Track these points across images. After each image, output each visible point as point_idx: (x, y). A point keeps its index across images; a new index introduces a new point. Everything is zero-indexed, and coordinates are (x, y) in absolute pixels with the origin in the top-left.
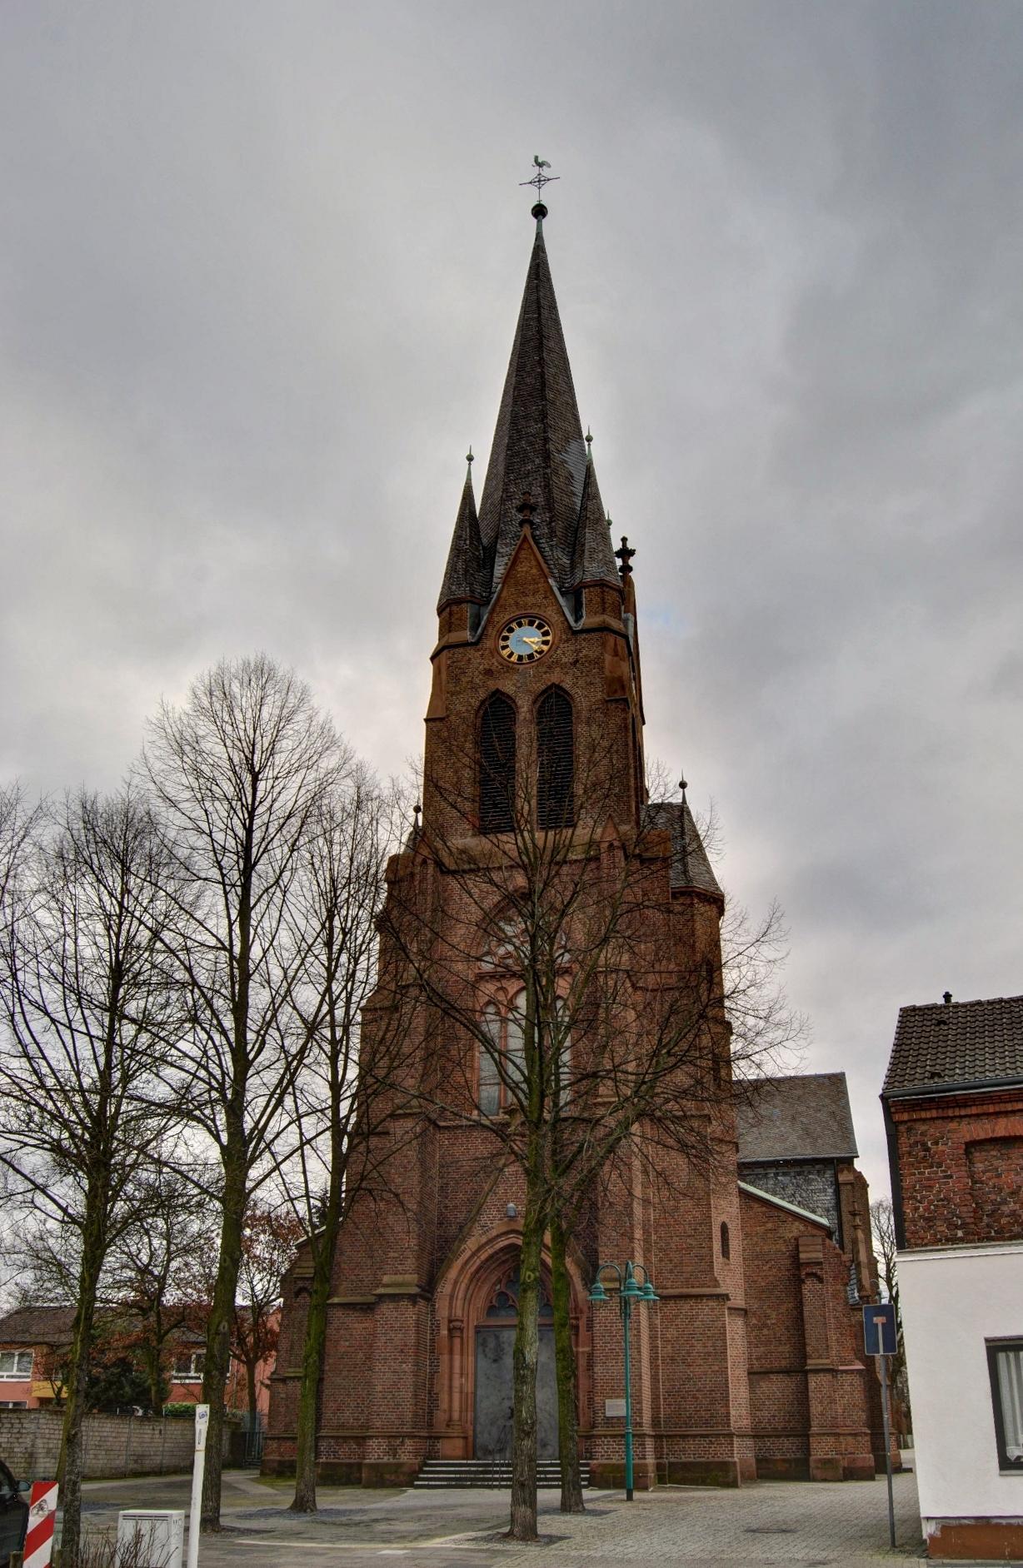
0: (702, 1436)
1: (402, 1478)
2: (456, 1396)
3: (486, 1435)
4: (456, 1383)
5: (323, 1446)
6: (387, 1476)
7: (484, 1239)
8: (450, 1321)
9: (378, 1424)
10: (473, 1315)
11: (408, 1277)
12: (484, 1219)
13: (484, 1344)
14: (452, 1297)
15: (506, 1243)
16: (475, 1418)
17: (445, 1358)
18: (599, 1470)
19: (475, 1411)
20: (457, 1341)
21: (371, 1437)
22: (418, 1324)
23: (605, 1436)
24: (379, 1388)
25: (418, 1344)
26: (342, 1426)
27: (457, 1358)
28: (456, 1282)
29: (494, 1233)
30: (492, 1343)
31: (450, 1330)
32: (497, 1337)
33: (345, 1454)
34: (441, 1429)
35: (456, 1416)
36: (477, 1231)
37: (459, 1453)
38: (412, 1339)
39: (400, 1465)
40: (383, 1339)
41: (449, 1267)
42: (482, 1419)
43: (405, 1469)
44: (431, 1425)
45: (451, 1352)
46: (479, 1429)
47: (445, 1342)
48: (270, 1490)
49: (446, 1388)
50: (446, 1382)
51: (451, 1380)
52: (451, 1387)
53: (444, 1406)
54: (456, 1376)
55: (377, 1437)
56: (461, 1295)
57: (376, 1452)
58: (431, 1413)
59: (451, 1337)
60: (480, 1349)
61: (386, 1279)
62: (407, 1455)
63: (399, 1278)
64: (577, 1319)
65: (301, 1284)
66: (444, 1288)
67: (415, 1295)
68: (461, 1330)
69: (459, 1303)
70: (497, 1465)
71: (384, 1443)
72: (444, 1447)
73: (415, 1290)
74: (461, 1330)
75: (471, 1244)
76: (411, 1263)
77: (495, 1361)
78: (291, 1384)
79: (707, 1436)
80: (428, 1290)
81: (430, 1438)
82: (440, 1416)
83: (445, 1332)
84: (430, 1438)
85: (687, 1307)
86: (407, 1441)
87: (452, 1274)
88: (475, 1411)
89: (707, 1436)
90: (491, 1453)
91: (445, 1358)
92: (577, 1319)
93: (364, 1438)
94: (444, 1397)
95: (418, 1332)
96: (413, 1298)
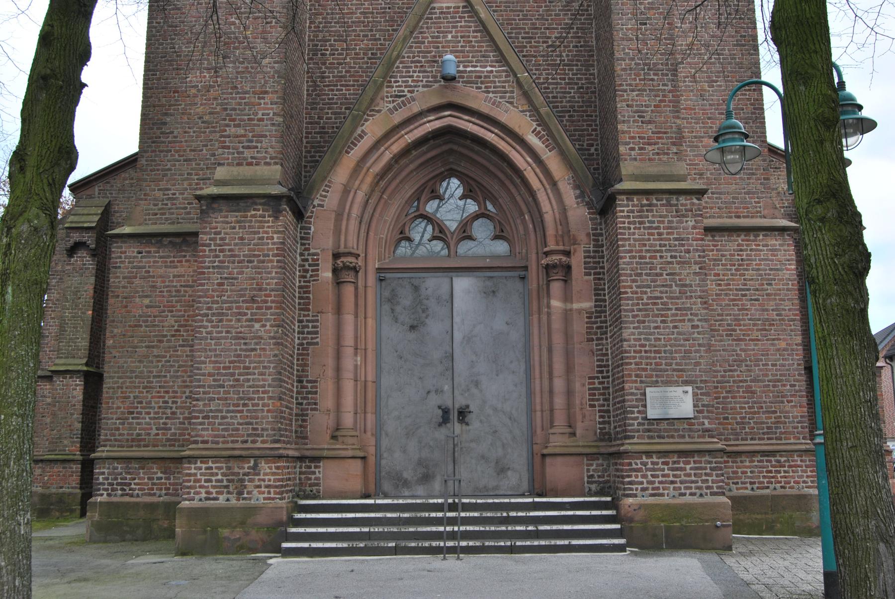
0: (764, 453)
1: (254, 535)
2: (348, 387)
3: (398, 455)
4: (348, 363)
5: (102, 474)
6: (225, 532)
7: (397, 118)
8: (336, 256)
9: (207, 434)
10: (373, 252)
11: (262, 171)
12: (398, 84)
13: (392, 300)
14: (339, 216)
15: (438, 124)
16: (379, 426)
17: (328, 320)
18: (640, 515)
19: (377, 412)
20: (348, 290)
21: (191, 459)
22: (282, 249)
23: (649, 454)
24: (209, 368)
25: (284, 287)
26: (137, 441)
27: (349, 319)
28: (346, 191)
29: (416, 108)
30: (406, 299)
31: (335, 271)
32: (416, 289)
33: (145, 486)
34: (320, 442)
35: (348, 420)
36: (385, 106)
37: (357, 485)
38: (272, 280)
39: (252, 511)
40: (216, 278)
41: (335, 163)
42: (391, 426)
43: (261, 518)
44: (302, 437)
45: (339, 310)
46: (385, 442)
47: (329, 291)
48: (650, 169)
49: (330, 372)
50: (330, 362)
51: (338, 357)
52: (338, 369)
53: (327, 401)
54: (348, 351)
55: (204, 459)
56: (356, 212)
57: (203, 488)
58: (302, 416)
59: (338, 283)
60: (386, 307)
61: (221, 173)
62: (265, 491)
63: (246, 171)
64: (568, 254)
65: (76, 237)
66: (325, 201)
67: (277, 198)
68: (355, 270)
69: (353, 224)
70: (467, 507)
71: (219, 470)
72: (328, 475)
73: (277, 190)
74: (355, 270)
75: (372, 128)
76: (270, 145)
77: (413, 328)
78: (58, 381)
79: (773, 453)
80: (295, 202)
81: (301, 459)
82: (320, 422)
83: (327, 274)
84: (301, 459)
85: (732, 246)
86: (264, 466)
87: (341, 175)
88: (377, 412)
89: (773, 453)
90: (406, 483)
91: (328, 320)
92: (568, 254)
93: (180, 460)
94: (326, 387)
95: (283, 266)
96: (272, 201)
